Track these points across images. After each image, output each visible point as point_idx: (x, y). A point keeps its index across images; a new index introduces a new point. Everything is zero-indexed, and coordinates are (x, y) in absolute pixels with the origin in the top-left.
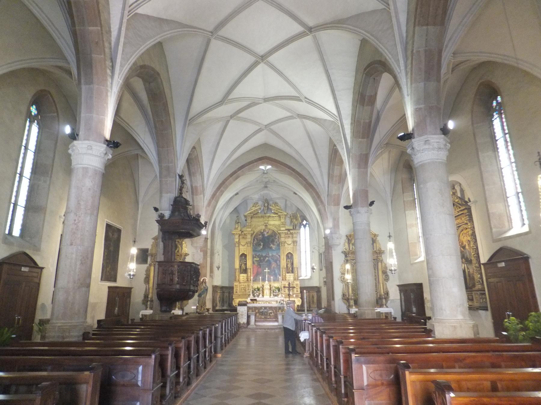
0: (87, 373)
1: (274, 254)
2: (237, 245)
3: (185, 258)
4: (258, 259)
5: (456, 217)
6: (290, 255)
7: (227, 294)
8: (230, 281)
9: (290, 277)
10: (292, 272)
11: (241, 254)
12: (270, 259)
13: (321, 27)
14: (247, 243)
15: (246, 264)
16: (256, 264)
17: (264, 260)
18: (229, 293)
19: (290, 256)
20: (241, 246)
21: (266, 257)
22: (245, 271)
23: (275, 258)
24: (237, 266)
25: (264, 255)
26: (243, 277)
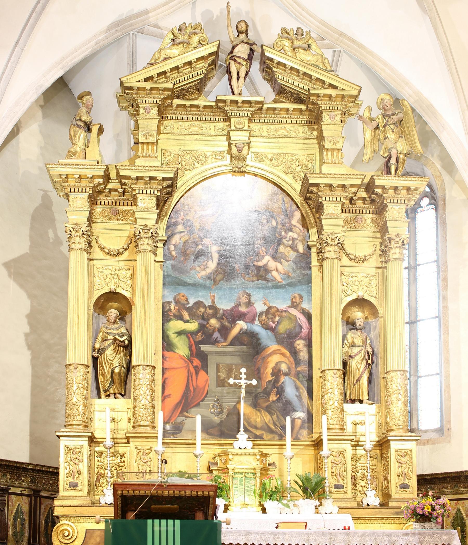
0: (211, 430)
1: (282, 304)
2: (80, 242)
3: (379, 407)
4: (193, 326)
5: (82, 448)
6: (358, 315)
7: (25, 503)
8: (35, 441)
9: (364, 420)
10: (372, 398)
11: (97, 294)
12: (257, 327)
13: (350, 84)
14: (134, 241)
15: (127, 347)
16: (182, 348)
17: (224, 331)
18: (35, 497)
19: (361, 312)
20: (97, 254)
21: (234, 316)
22: (122, 383)
23: (284, 327)
24: (78, 351)
25: (224, 305)
26: (109, 415)
